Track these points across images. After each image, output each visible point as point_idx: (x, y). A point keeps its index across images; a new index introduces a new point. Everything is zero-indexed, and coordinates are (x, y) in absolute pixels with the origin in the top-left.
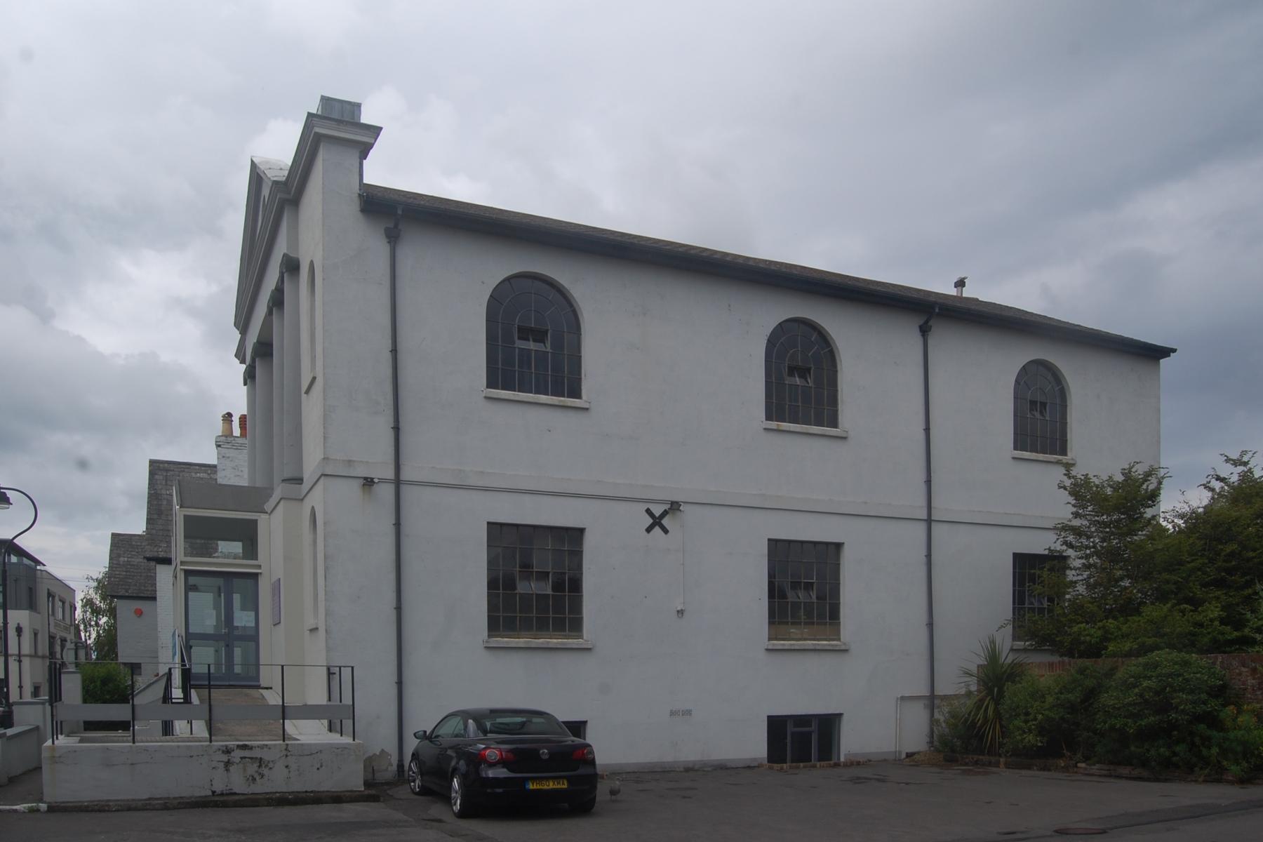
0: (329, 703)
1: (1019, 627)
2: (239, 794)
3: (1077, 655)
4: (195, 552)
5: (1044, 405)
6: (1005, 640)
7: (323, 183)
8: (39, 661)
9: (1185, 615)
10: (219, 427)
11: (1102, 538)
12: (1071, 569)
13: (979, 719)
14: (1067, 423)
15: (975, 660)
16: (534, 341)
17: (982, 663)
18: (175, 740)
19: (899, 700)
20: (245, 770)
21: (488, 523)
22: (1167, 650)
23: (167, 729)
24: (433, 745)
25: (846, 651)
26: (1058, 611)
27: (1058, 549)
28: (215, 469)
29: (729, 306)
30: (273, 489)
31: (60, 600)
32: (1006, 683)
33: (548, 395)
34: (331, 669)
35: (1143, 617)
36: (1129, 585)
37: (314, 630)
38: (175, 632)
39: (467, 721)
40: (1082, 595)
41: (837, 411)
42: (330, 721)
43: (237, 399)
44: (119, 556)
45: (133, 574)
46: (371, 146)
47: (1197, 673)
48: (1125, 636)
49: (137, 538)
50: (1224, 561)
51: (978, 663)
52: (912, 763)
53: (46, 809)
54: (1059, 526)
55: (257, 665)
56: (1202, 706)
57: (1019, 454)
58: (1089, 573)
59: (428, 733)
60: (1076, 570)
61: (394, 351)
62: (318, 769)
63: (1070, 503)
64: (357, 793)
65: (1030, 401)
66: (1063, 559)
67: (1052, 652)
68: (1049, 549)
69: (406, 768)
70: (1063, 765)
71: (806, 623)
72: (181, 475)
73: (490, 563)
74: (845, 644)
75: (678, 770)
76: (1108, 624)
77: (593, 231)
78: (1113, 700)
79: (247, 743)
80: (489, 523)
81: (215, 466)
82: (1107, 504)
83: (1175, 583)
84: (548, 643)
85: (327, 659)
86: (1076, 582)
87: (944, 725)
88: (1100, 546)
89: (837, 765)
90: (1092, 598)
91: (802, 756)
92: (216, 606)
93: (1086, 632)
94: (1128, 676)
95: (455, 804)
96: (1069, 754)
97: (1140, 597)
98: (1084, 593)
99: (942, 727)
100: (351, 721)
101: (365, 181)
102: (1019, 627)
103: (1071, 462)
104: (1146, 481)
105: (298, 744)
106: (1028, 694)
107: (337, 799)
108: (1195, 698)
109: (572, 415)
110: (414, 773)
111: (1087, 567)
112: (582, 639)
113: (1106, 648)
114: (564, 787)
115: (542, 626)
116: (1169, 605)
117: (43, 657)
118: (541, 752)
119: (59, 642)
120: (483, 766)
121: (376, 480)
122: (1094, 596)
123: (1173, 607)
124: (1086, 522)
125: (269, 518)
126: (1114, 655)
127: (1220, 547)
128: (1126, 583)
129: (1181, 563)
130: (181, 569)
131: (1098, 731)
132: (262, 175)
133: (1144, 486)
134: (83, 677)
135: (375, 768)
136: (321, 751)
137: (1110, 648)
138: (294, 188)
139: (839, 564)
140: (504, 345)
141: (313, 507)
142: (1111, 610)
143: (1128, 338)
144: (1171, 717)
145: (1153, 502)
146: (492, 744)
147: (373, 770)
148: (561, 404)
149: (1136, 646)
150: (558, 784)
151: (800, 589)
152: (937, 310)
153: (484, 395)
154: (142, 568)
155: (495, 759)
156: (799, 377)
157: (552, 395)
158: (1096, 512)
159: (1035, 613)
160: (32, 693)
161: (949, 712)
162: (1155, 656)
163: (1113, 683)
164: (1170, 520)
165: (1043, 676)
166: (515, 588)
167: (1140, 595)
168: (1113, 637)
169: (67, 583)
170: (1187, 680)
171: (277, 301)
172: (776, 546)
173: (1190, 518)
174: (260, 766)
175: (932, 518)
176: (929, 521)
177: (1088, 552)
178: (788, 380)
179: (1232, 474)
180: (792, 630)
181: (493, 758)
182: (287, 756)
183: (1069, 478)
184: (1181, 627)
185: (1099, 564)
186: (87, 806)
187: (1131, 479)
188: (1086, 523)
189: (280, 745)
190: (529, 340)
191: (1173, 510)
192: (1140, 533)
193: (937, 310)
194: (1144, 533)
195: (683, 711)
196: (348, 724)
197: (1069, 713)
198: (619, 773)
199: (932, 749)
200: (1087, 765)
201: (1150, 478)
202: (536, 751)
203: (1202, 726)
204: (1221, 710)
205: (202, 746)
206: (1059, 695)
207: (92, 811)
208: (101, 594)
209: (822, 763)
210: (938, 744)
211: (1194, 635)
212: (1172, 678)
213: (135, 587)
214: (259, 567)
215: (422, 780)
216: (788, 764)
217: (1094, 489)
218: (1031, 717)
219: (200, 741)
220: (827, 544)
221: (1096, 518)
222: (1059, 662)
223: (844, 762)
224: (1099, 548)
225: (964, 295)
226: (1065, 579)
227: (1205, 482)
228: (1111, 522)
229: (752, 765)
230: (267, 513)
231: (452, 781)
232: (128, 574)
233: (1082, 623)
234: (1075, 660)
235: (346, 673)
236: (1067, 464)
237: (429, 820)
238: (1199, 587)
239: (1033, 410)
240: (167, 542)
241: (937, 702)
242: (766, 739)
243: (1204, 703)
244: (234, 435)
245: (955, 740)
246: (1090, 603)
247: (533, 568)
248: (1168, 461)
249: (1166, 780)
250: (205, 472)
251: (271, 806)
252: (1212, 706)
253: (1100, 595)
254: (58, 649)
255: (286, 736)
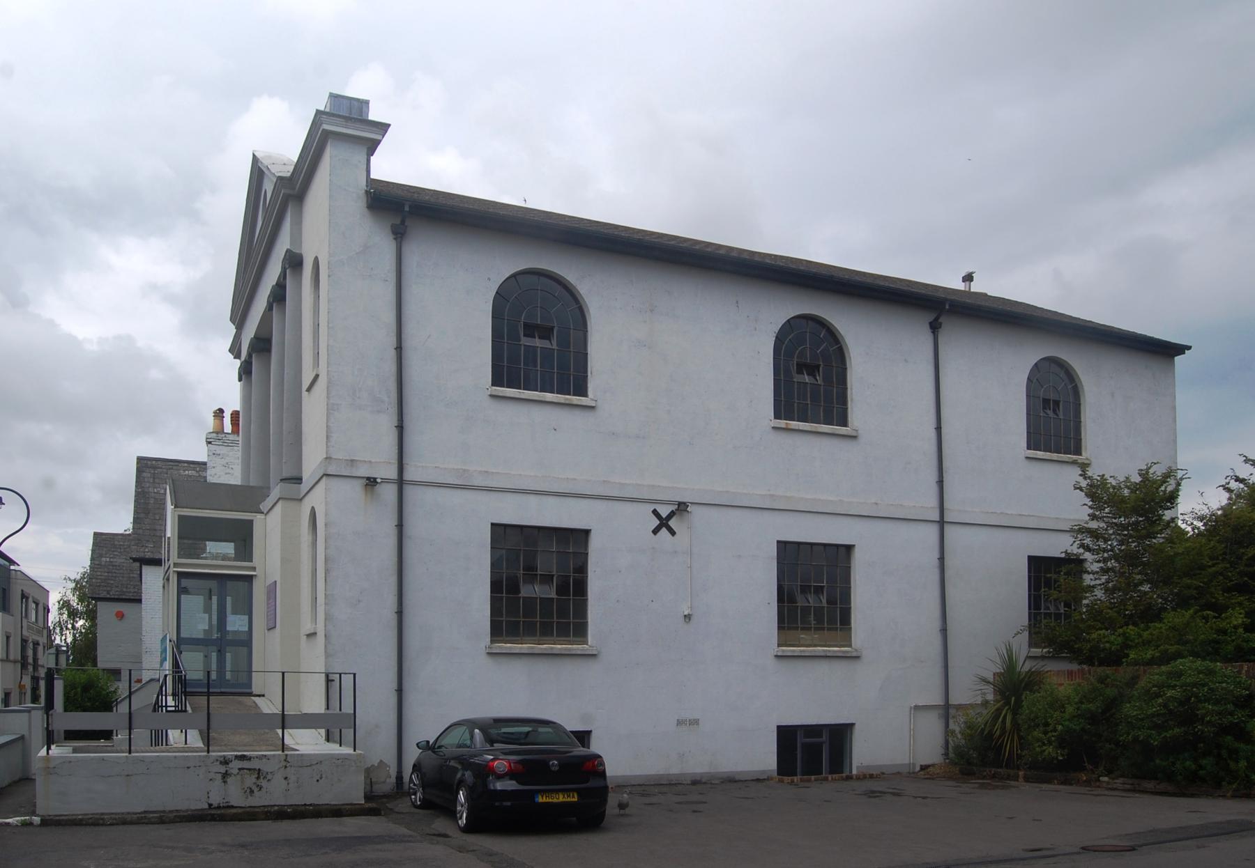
0: (328, 712)
1: (1035, 633)
2: (236, 807)
3: (1096, 663)
4: (182, 553)
5: (1057, 403)
6: (1021, 646)
7: (330, 180)
8: (10, 666)
9: (1208, 622)
10: (210, 422)
11: (1119, 541)
12: (1089, 573)
13: (997, 730)
14: (1080, 422)
15: (992, 667)
16: (540, 338)
17: (998, 671)
18: (171, 750)
19: (912, 710)
20: (242, 782)
21: (492, 524)
22: (1191, 658)
23: (158, 738)
24: (438, 757)
25: (858, 657)
26: (1076, 616)
27: (1075, 552)
28: (204, 467)
29: (737, 302)
30: (269, 488)
31: (34, 602)
32: (1025, 692)
33: (554, 393)
34: (330, 675)
35: (1164, 623)
36: (1149, 590)
37: (312, 635)
38: (165, 636)
39: (473, 731)
40: (1100, 600)
41: (847, 409)
42: (328, 730)
43: (231, 396)
44: (101, 556)
45: (114, 575)
46: (379, 142)
47: (1223, 683)
48: (1147, 643)
49: (120, 537)
50: (1246, 565)
51: (994, 671)
52: (926, 776)
53: (39, 823)
54: (1076, 528)
55: (250, 672)
56: (1229, 717)
57: (1032, 453)
58: (1107, 577)
59: (431, 743)
60: (1094, 574)
61: (399, 348)
62: (318, 781)
63: (1087, 505)
64: (357, 806)
65: (1043, 399)
66: (1079, 562)
67: (1071, 660)
68: (1066, 552)
69: (406, 779)
70: (1085, 778)
71: (816, 629)
72: (169, 472)
73: (493, 565)
74: (856, 650)
75: (684, 782)
76: (1128, 630)
77: (597, 226)
78: (1136, 710)
79: (245, 753)
80: (492, 524)
81: (205, 464)
82: (1124, 506)
83: (1196, 589)
84: (552, 648)
85: (326, 666)
86: (1094, 587)
87: (959, 736)
88: (1119, 549)
89: (849, 778)
90: (1111, 603)
91: (812, 768)
92: (207, 609)
93: (1106, 639)
94: (1151, 685)
95: (461, 818)
96: (1091, 767)
97: (1161, 603)
98: (1102, 599)
99: (957, 738)
100: (352, 730)
101: (373, 176)
102: (1035, 633)
103: (1086, 462)
104: (1165, 482)
105: (298, 755)
106: (1047, 704)
107: (337, 812)
108: (1221, 709)
109: (577, 413)
110: (415, 785)
111: (1104, 571)
112: (587, 644)
113: (1127, 656)
114: (574, 800)
115: (548, 631)
116: (1191, 611)
117: (15, 662)
118: (551, 763)
119: (31, 645)
120: (491, 778)
121: (379, 480)
122: (1112, 601)
123: (1195, 613)
124: (1104, 524)
125: (266, 519)
126: (1136, 663)
127: (1242, 550)
128: (1146, 588)
129: (1202, 568)
130: (174, 571)
131: (1121, 743)
132: (265, 170)
133: (1163, 488)
134: (65, 682)
135: (373, 780)
136: (321, 762)
137: (1132, 656)
138: (298, 185)
139: (850, 567)
140: (510, 342)
141: (313, 508)
142: (1131, 616)
143: (1141, 334)
144: (1196, 729)
145: (1172, 504)
146: (500, 755)
147: (371, 782)
148: (567, 402)
149: (1157, 654)
150: (568, 797)
151: (810, 593)
152: (947, 307)
153: (489, 393)
154: (124, 568)
155: (503, 771)
156: (808, 374)
157: (557, 393)
158: (1114, 514)
159: (1051, 619)
160: (2, 699)
161: (965, 723)
162: (1179, 664)
163: (1135, 692)
164: (1189, 522)
165: (1063, 684)
166: (519, 592)
167: (1160, 600)
168: (1134, 645)
169: (41, 583)
170: (1212, 690)
171: (279, 296)
172: (784, 547)
173: (1209, 520)
174: (258, 778)
175: (945, 520)
176: (942, 523)
177: (1106, 555)
178: (797, 378)
179: (1251, 474)
180: (802, 636)
181: (501, 769)
182: (286, 767)
183: (1085, 478)
184: (1204, 634)
185: (1118, 569)
186: (81, 820)
187: (1149, 481)
188: (1103, 525)
189: (279, 755)
190: (535, 338)
191: (1192, 512)
192: (1159, 535)
193: (947, 307)
194: (1163, 535)
195: (690, 720)
196: (347, 734)
197: (1089, 724)
198: (621, 787)
199: (947, 761)
200: (1110, 778)
201: (1169, 480)
202: (545, 764)
203: (1229, 737)
204: (1248, 722)
205: (200, 756)
206: (1080, 705)
207: (87, 824)
208: (79, 595)
209: (834, 776)
210: (953, 755)
211: (1217, 642)
212: (1197, 688)
213: (117, 589)
214: (254, 569)
215: (424, 793)
216: (799, 777)
217: (1111, 490)
218: (1051, 728)
219: (197, 752)
220: (837, 546)
221: (1114, 521)
222: (1079, 669)
223: (856, 776)
224: (1117, 551)
225: (972, 290)
226: (1082, 583)
227: (1224, 484)
228: (1129, 524)
229: (761, 778)
230: (263, 513)
231: (458, 793)
232: (110, 574)
233: (1101, 629)
234: (1094, 668)
235: (347, 681)
236: (1084, 464)
237: (434, 835)
238: (1221, 592)
239: (1046, 409)
240: (154, 542)
241: (952, 712)
242: (776, 750)
243: (1231, 714)
244: (225, 431)
245: (971, 752)
246: (1109, 608)
247: (536, 571)
248: (1184, 460)
249: (1192, 796)
250: (194, 469)
251: (269, 820)
252: (1238, 718)
253: (1119, 600)
254: (30, 653)
255: (285, 746)
